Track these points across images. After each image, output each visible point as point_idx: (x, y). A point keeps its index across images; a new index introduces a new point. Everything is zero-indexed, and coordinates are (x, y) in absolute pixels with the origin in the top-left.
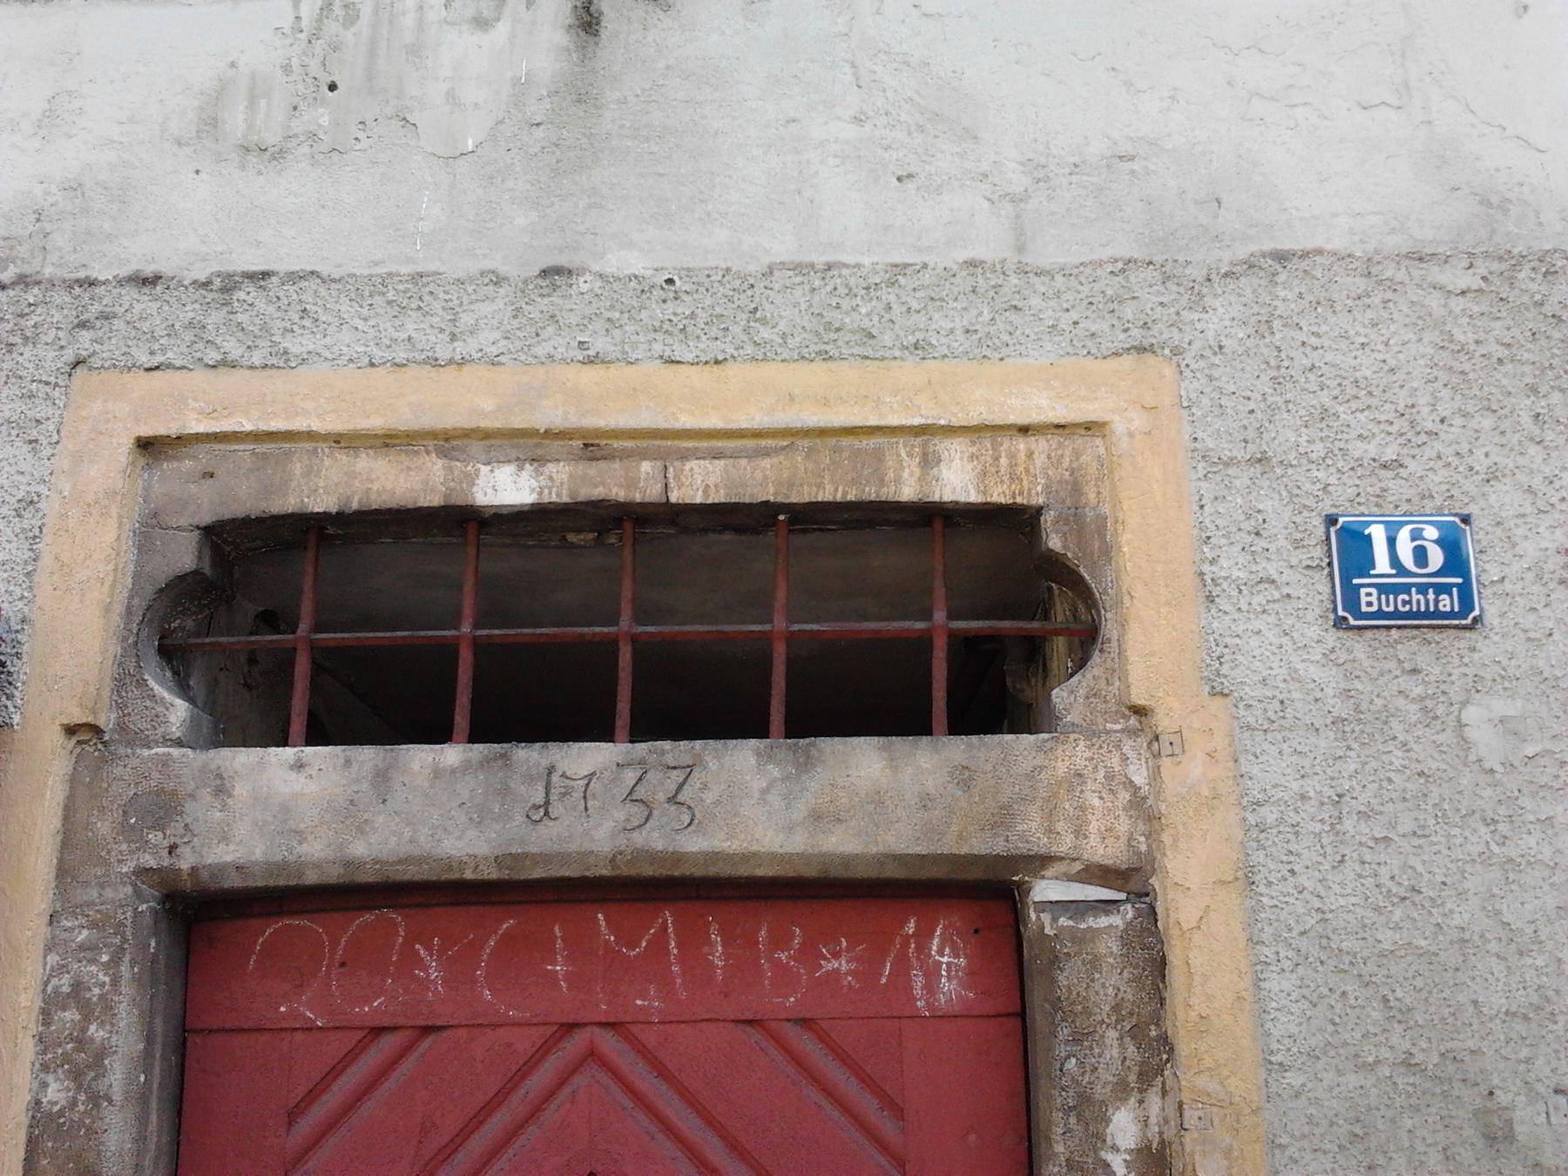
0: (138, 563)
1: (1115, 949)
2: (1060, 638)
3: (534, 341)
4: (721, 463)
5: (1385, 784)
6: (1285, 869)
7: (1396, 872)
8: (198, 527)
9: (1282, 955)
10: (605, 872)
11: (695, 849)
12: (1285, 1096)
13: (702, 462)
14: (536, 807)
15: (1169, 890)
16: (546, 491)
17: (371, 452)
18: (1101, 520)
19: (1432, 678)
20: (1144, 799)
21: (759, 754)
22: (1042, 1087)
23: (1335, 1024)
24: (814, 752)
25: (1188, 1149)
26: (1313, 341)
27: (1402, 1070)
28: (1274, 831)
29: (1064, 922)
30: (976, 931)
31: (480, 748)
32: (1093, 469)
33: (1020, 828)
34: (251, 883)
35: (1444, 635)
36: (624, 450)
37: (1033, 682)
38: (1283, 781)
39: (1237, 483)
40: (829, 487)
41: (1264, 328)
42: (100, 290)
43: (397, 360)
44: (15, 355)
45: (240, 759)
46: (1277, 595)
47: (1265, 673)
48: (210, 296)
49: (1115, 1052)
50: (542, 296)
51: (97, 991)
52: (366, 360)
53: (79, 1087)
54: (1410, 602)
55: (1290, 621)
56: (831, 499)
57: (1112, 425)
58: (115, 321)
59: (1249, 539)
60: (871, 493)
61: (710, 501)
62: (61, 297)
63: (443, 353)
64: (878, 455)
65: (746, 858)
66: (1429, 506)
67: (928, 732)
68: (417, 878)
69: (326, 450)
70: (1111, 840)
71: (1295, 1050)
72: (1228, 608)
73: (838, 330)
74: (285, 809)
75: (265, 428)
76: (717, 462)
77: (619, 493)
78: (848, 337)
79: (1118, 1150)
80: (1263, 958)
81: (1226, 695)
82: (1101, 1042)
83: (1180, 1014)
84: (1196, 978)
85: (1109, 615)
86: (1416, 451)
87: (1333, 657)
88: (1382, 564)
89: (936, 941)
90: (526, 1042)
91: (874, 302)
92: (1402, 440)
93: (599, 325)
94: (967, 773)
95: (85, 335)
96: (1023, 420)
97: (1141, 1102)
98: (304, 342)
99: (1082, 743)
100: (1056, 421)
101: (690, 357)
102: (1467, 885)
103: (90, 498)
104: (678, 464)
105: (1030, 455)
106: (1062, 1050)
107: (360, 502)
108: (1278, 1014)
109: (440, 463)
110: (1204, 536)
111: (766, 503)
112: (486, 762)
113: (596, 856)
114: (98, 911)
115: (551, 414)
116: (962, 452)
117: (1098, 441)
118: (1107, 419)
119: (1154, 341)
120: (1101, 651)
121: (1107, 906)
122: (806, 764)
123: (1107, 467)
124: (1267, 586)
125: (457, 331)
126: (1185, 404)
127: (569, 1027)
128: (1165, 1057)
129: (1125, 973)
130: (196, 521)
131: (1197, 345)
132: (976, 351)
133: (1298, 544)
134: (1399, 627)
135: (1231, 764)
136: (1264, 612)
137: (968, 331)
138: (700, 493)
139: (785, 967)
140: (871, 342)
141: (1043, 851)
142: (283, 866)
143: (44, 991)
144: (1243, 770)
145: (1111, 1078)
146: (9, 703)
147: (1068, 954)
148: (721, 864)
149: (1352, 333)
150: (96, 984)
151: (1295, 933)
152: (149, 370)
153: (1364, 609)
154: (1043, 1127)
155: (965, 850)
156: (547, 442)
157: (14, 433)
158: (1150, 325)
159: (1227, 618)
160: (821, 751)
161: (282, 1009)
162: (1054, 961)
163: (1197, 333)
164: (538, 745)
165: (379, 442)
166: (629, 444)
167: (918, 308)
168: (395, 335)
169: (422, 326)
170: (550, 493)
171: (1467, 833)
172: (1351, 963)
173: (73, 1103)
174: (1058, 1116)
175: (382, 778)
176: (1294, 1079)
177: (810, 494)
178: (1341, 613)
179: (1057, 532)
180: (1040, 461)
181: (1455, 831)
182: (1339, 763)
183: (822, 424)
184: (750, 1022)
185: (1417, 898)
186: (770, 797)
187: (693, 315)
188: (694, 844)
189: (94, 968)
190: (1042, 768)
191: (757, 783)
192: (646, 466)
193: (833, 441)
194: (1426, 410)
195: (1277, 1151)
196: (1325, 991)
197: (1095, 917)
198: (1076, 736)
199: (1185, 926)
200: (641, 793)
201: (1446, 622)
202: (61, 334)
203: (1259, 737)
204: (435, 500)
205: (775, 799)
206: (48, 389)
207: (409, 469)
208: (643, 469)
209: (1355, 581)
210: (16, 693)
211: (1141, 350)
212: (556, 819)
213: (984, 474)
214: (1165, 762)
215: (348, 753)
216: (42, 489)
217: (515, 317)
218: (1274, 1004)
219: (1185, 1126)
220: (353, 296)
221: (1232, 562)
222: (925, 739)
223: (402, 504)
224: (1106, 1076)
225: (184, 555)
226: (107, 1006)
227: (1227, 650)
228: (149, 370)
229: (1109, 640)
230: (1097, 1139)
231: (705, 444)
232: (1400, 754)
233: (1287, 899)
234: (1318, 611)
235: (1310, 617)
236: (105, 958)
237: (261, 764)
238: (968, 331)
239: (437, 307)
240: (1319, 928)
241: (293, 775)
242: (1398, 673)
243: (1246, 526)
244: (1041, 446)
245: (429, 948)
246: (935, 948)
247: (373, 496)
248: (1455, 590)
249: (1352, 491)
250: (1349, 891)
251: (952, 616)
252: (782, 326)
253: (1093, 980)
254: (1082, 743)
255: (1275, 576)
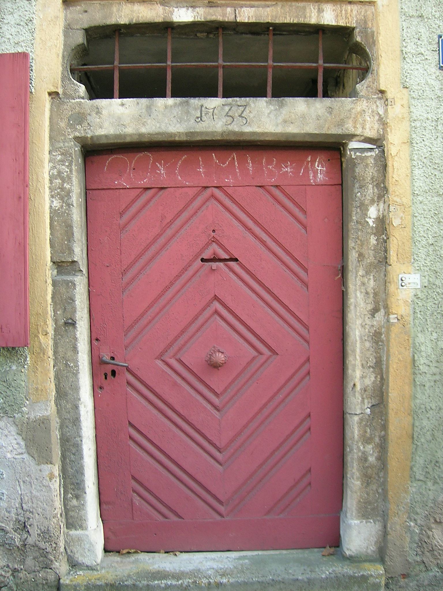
1: (372, 162)
4: (253, 9)
9: (419, 164)
10: (219, 138)
11: (248, 131)
12: (418, 203)
14: (198, 118)
15: (389, 145)
18: (373, 33)
20: (382, 118)
21: (267, 102)
23: (432, 183)
24: (284, 102)
25: (390, 217)
30: (329, 160)
31: (178, 100)
32: (371, 17)
34: (110, 142)
36: (222, 4)
38: (422, 114)
39: (414, 23)
40: (288, 18)
46: (423, 58)
47: (419, 82)
49: (371, 191)
51: (65, 174)
53: (63, 202)
55: (427, 66)
57: (377, 2)
59: (416, 41)
60: (302, 20)
61: (250, 21)
65: (263, 134)
70: (372, 131)
71: (421, 190)
74: (119, 118)
76: (252, 8)
77: (220, 18)
79: (371, 218)
80: (414, 165)
81: (407, 88)
82: (367, 189)
83: (390, 180)
84: (395, 170)
87: (438, 78)
89: (317, 163)
90: (191, 192)
97: (378, 205)
104: (239, 9)
105: (352, 11)
106: (356, 191)
108: (417, 180)
109: (161, 7)
110: (403, 39)
112: (181, 104)
113: (217, 133)
114: (64, 150)
116: (331, 9)
117: (373, 7)
121: (371, 150)
122: (282, 106)
123: (375, 16)
124: (421, 55)
127: (206, 188)
128: (385, 192)
129: (375, 169)
133: (430, 43)
135: (408, 109)
136: (420, 63)
138: (247, 18)
139: (272, 171)
141: (353, 133)
142: (119, 136)
143: (49, 174)
144: (411, 110)
145: (370, 198)
147: (359, 163)
151: (423, 158)
155: (330, 132)
159: (409, 64)
160: (286, 102)
161: (116, 182)
162: (354, 165)
164: (197, 99)
170: (198, 18)
172: (438, 167)
173: (62, 206)
174: (354, 209)
175: (149, 108)
177: (282, 20)
178: (441, 65)
180: (355, 12)
182: (438, 109)
186: (270, 116)
188: (247, 129)
189: (64, 167)
190: (353, 108)
191: (267, 111)
195: (414, 218)
196: (430, 174)
197: (367, 152)
198: (363, 99)
199: (393, 155)
200: (230, 114)
205: (272, 116)
207: (151, 9)
208: (228, 10)
212: (204, 121)
213: (337, 16)
214: (389, 107)
215: (138, 101)
218: (416, 177)
219: (391, 211)
221: (411, 48)
223: (150, 21)
226: (69, 178)
227: (408, 74)
230: (365, 215)
233: (422, 148)
234: (435, 64)
235: (432, 66)
236: (67, 164)
241: (121, 108)
245: (161, 164)
246: (316, 165)
247: (140, 18)
250: (439, 146)
253: (366, 171)
254: (365, 101)
255: (423, 53)
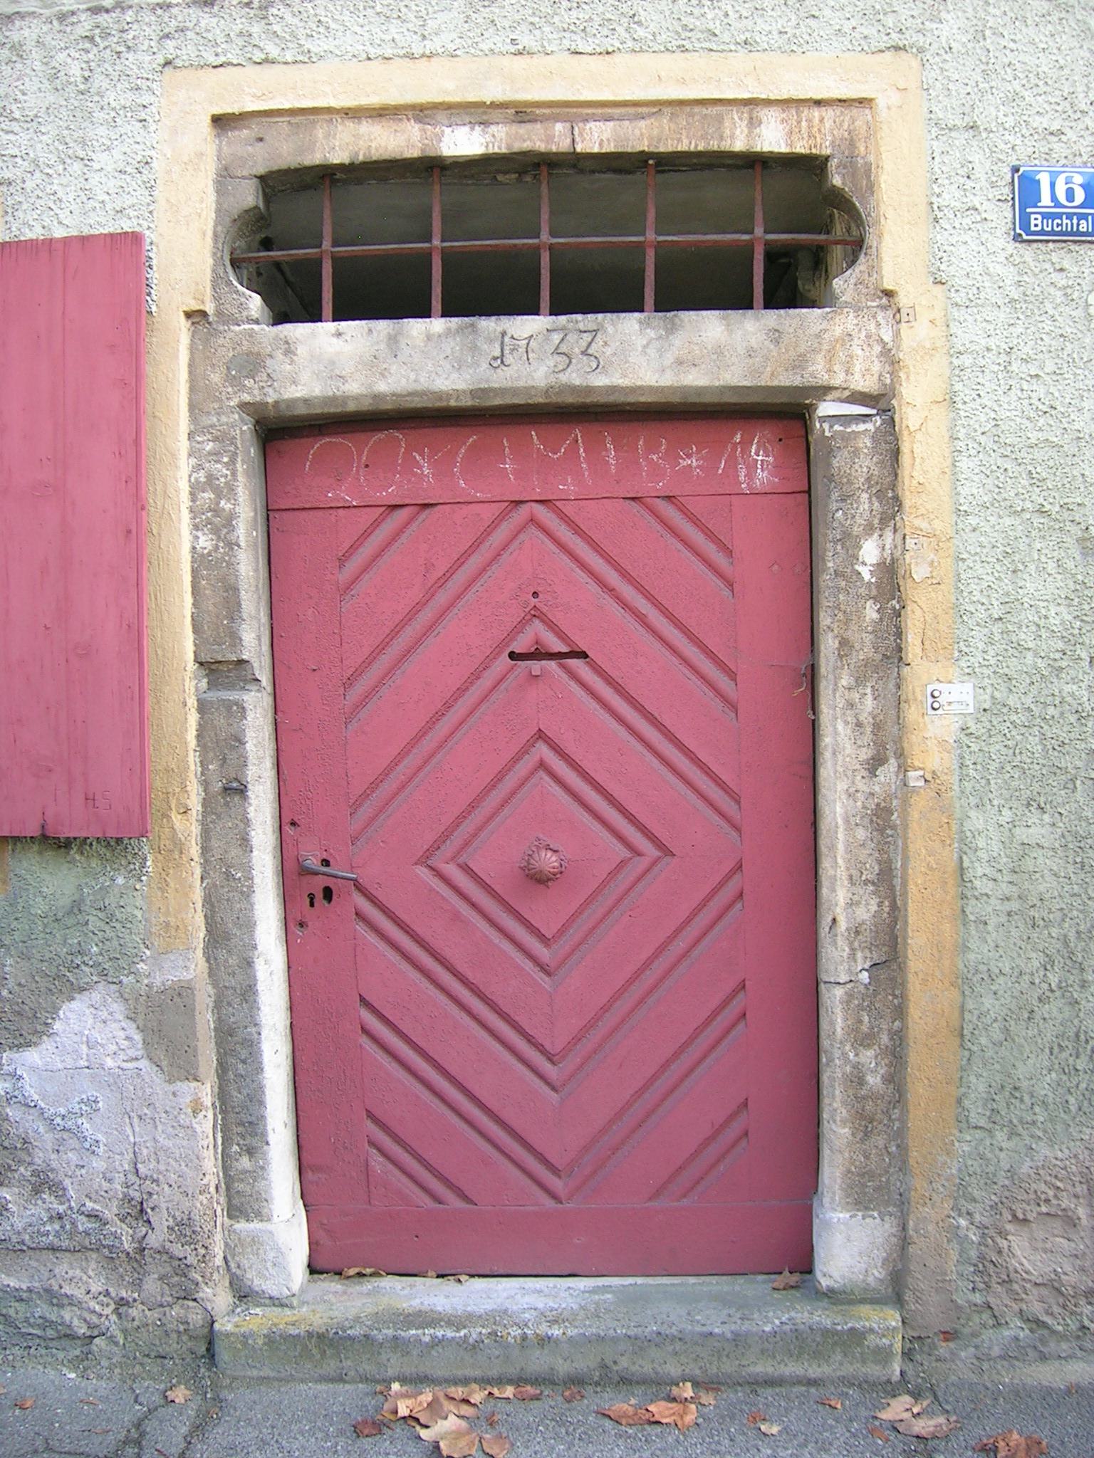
0: (218, 202)
1: (869, 444)
2: (839, 246)
3: (479, 39)
5: (1039, 342)
6: (974, 394)
7: (1042, 396)
8: (256, 176)
9: (970, 446)
10: (541, 400)
11: (601, 384)
13: (598, 123)
14: (495, 359)
16: (491, 145)
17: (369, 120)
18: (868, 166)
19: (1072, 275)
20: (890, 350)
22: (819, 530)
24: (677, 320)
25: (907, 562)
26: (1012, 45)
27: (1036, 515)
28: (969, 370)
29: (837, 427)
32: (863, 131)
33: (810, 369)
35: (1082, 247)
37: (817, 284)
39: (957, 142)
40: (686, 141)
41: (979, 35)
42: (175, 11)
43: (386, 55)
44: (123, 60)
45: (298, 331)
46: (979, 219)
48: (252, 12)
49: (866, 507)
50: (484, 6)
52: (365, 56)
53: (219, 537)
54: (1061, 225)
56: (687, 149)
58: (188, 33)
60: (714, 145)
62: (148, 17)
63: (417, 50)
64: (720, 120)
65: (633, 390)
66: (1079, 161)
67: (749, 306)
68: (419, 406)
69: (339, 120)
70: (867, 377)
72: (947, 226)
73: (691, 30)
75: (299, 106)
77: (541, 146)
78: (699, 35)
82: (858, 502)
83: (906, 482)
85: (871, 230)
86: (1072, 124)
87: (1011, 259)
88: (1046, 199)
91: (716, 11)
92: (1064, 116)
93: (524, 27)
94: (777, 334)
95: (170, 44)
96: (818, 96)
97: (881, 536)
98: (321, 44)
99: (851, 315)
100: (839, 97)
101: (589, 50)
102: (1084, 404)
103: (185, 159)
104: (581, 125)
105: (822, 120)
106: (834, 506)
107: (364, 154)
109: (417, 126)
111: (643, 152)
112: (460, 330)
115: (493, 92)
117: (867, 111)
118: (873, 96)
119: (906, 43)
120: (866, 254)
122: (672, 329)
125: (426, 33)
126: (925, 87)
127: (518, 503)
130: (254, 172)
131: (935, 46)
132: (787, 47)
133: (993, 185)
134: (1054, 241)
135: (944, 328)
137: (781, 33)
138: (597, 145)
140: (715, 39)
141: (825, 383)
142: (333, 399)
143: (190, 481)
144: (952, 332)
146: (148, 298)
147: (839, 448)
148: (617, 394)
149: (1037, 40)
150: (222, 476)
151: (979, 433)
152: (215, 67)
153: (1033, 228)
154: (820, 553)
155: (775, 383)
156: (490, 110)
157: (129, 115)
158: (904, 30)
159: (946, 233)
162: (830, 452)
163: (935, 38)
164: (493, 318)
165: (374, 113)
166: (547, 111)
167: (746, 15)
168: (384, 37)
169: (402, 30)
171: (1086, 373)
173: (217, 547)
174: (829, 545)
175: (393, 340)
176: (973, 521)
178: (1018, 231)
179: (839, 174)
180: (828, 124)
181: (1078, 371)
182: (1011, 328)
183: (681, 97)
184: (633, 499)
185: (1053, 412)
186: (648, 351)
187: (591, 19)
188: (600, 381)
189: (219, 466)
190: (826, 331)
191: (640, 342)
192: (559, 127)
193: (688, 109)
194: (1081, 96)
195: (960, 563)
196: (994, 468)
197: (857, 424)
199: (912, 429)
200: (563, 348)
201: (1084, 238)
202: (153, 44)
203: (963, 310)
204: (414, 153)
205: (651, 351)
206: (149, 83)
209: (1029, 210)
210: (152, 291)
211: (897, 48)
216: (152, 153)
217: (466, 22)
218: (964, 476)
220: (352, 9)
222: (750, 312)
223: (393, 155)
224: (859, 521)
225: (249, 196)
226: (231, 489)
228: (215, 67)
229: (871, 247)
231: (600, 111)
232: (1049, 323)
234: (1004, 229)
235: (998, 233)
237: (313, 334)
238: (781, 33)
239: (411, 16)
240: (994, 430)
241: (335, 340)
242: (1052, 270)
243: (962, 172)
244: (829, 113)
247: (373, 151)
248: (1090, 218)
249: (1031, 150)
251: (766, 232)
252: (653, 27)
254: (851, 315)
255: (978, 206)
